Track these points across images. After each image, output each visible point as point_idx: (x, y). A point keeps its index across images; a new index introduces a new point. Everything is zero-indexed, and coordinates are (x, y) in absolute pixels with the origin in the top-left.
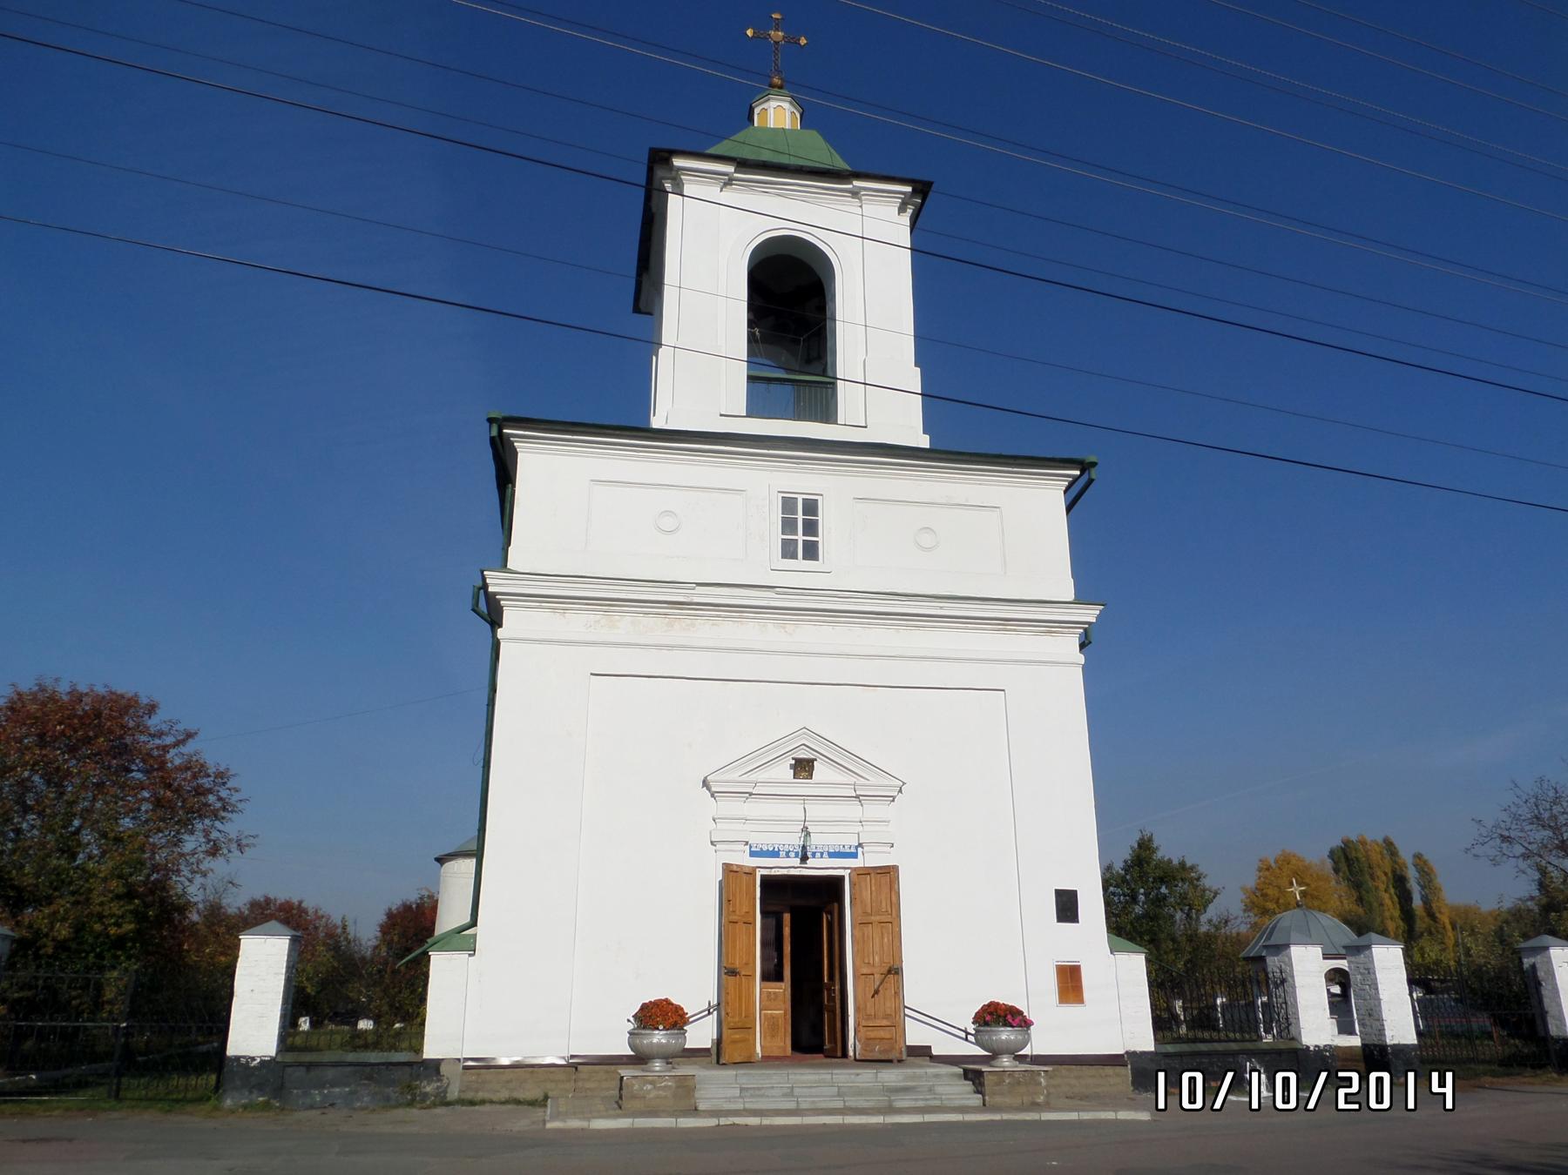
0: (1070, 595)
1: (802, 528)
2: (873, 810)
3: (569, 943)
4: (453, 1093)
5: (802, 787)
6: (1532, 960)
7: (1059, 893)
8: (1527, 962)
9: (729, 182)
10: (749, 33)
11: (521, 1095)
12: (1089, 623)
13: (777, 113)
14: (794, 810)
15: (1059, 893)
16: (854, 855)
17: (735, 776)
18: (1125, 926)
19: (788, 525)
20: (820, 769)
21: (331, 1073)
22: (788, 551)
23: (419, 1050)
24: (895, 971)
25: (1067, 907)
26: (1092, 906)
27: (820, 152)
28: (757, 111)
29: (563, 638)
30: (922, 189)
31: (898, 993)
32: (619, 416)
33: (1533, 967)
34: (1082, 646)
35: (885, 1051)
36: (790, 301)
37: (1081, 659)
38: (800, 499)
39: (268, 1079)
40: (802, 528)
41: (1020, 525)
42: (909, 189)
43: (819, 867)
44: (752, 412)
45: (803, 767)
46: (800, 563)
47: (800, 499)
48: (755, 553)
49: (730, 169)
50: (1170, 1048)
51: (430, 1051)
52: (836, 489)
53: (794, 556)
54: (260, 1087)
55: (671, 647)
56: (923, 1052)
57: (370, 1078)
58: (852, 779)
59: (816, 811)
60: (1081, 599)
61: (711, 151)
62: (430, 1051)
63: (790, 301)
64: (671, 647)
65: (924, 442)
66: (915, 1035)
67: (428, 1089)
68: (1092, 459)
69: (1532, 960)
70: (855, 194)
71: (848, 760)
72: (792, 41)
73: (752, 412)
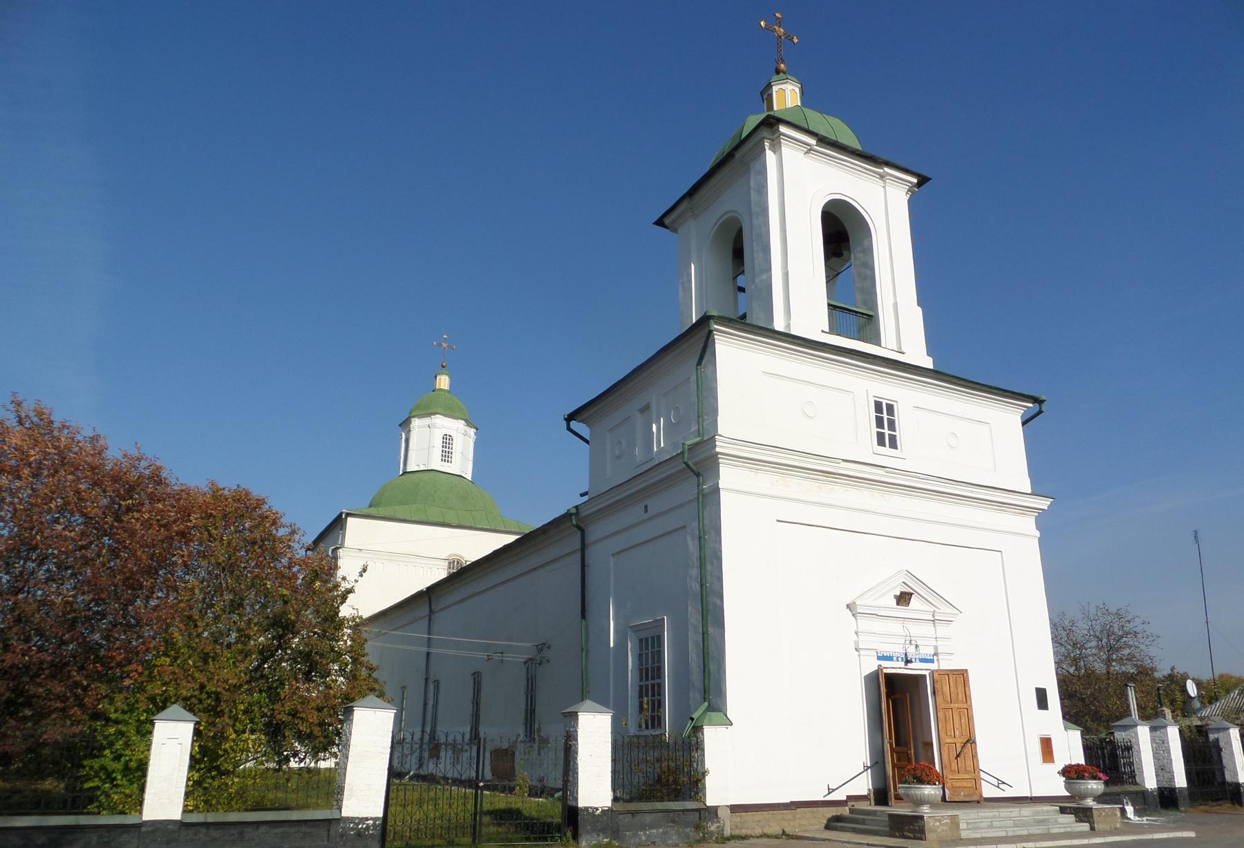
2: (942, 630)
4: (727, 833)
5: (902, 611)
6: (1216, 736)
8: (1212, 737)
9: (810, 150)
10: (762, 23)
11: (769, 831)
14: (896, 627)
16: (932, 661)
18: (1071, 716)
20: (914, 601)
21: (648, 818)
23: (702, 800)
24: (971, 741)
25: (1042, 702)
30: (923, 181)
31: (974, 756)
33: (1217, 740)
35: (969, 795)
38: (884, 402)
39: (606, 821)
41: (984, 437)
42: (915, 181)
43: (916, 668)
45: (904, 598)
46: (887, 450)
48: (863, 443)
49: (813, 141)
51: (710, 802)
53: (884, 445)
54: (603, 830)
57: (673, 821)
62: (710, 802)
64: (830, 505)
65: (928, 363)
67: (713, 828)
68: (1043, 398)
69: (1216, 736)
70: (882, 177)
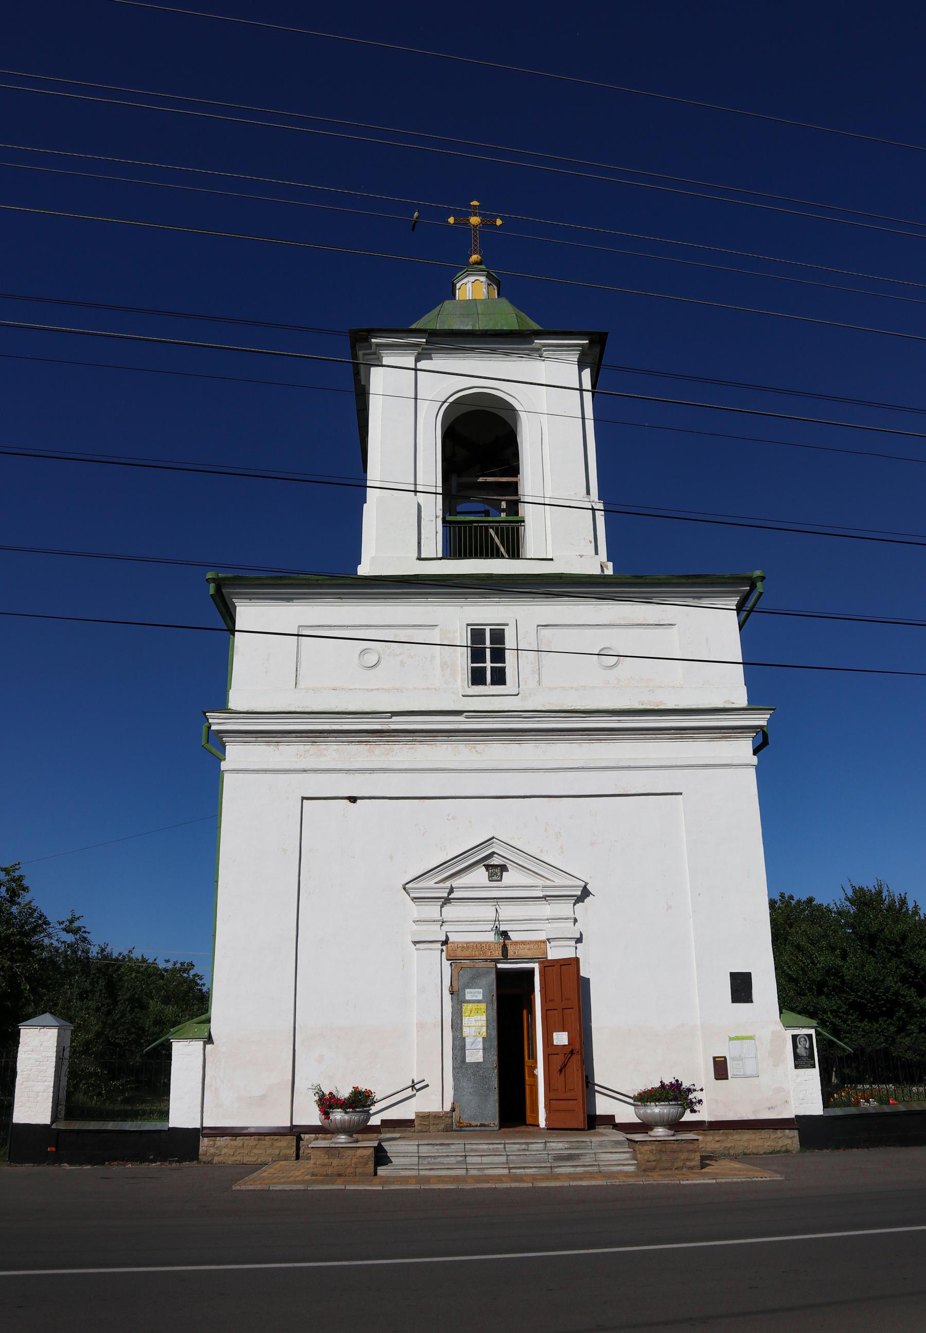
0: (743, 702)
1: (487, 657)
3: (315, 999)
7: (733, 976)
12: (761, 727)
13: (472, 287)
14: (486, 912)
15: (733, 976)
17: (431, 883)
19: (477, 655)
22: (477, 677)
25: (741, 987)
26: (765, 986)
27: (508, 317)
28: (458, 286)
29: (271, 767)
32: (326, 565)
34: (755, 752)
36: (480, 446)
37: (754, 760)
38: (488, 629)
40: (487, 657)
41: (695, 647)
44: (453, 550)
47: (488, 629)
48: (442, 680)
50: (838, 1111)
52: (518, 618)
53: (484, 683)
55: (373, 771)
56: (609, 1120)
58: (540, 882)
59: (508, 911)
60: (753, 706)
61: (413, 327)
63: (480, 446)
66: (603, 1106)
71: (535, 864)
72: (487, 224)
73: (453, 550)
